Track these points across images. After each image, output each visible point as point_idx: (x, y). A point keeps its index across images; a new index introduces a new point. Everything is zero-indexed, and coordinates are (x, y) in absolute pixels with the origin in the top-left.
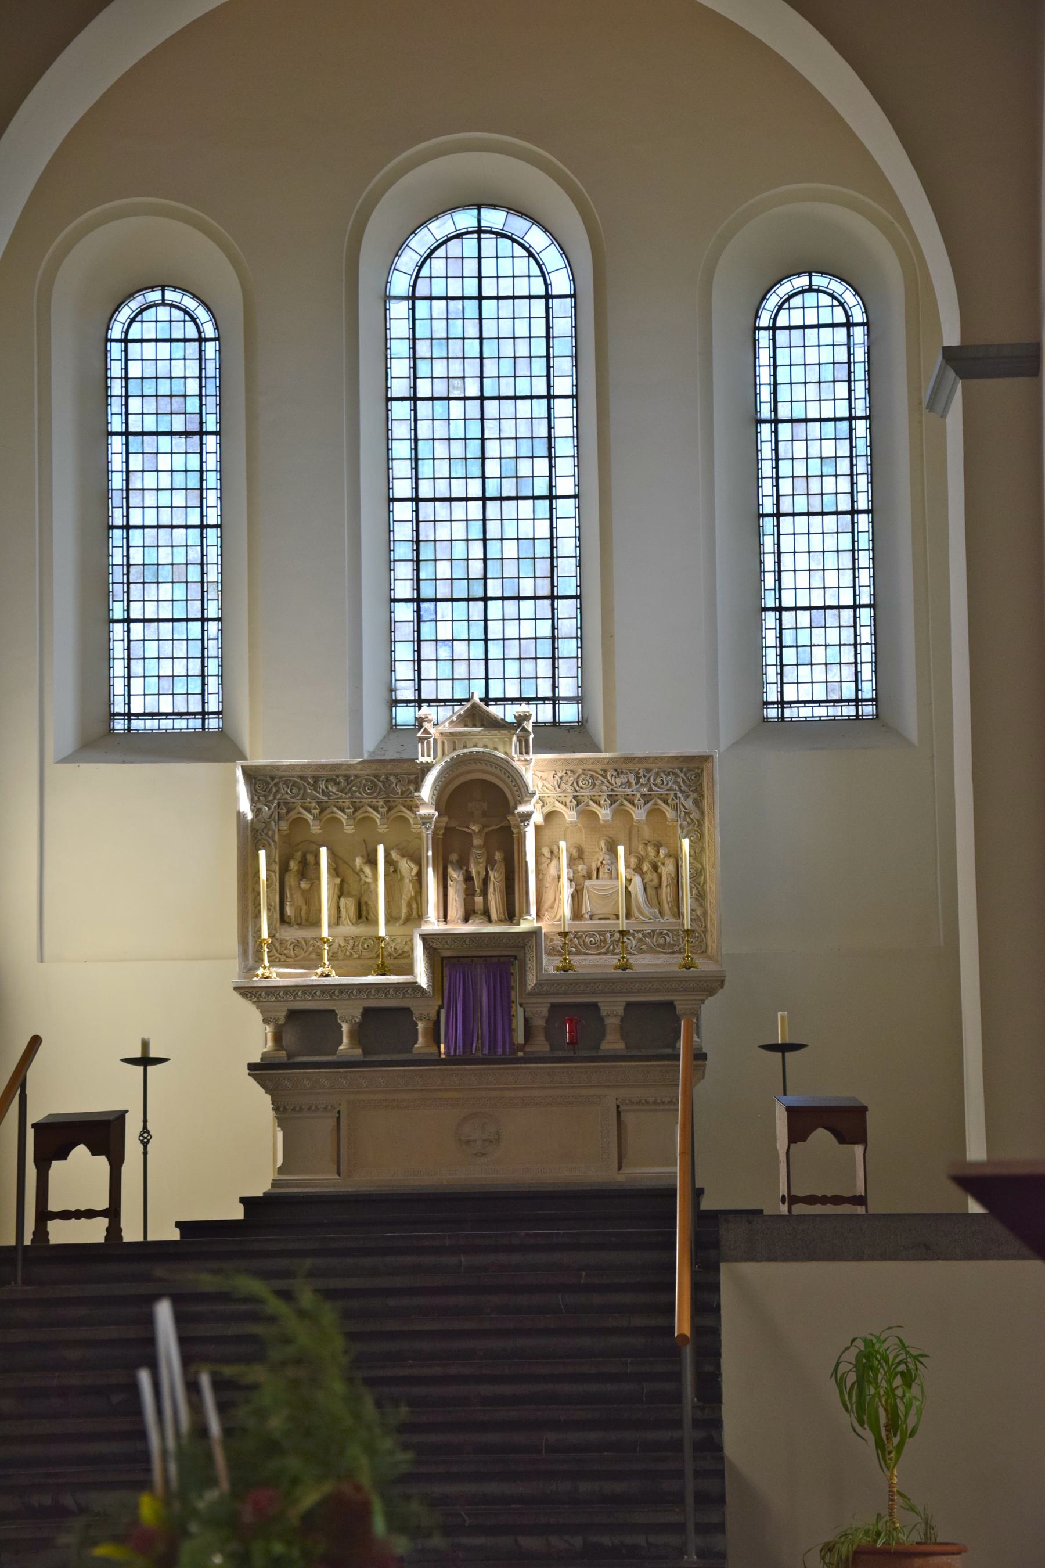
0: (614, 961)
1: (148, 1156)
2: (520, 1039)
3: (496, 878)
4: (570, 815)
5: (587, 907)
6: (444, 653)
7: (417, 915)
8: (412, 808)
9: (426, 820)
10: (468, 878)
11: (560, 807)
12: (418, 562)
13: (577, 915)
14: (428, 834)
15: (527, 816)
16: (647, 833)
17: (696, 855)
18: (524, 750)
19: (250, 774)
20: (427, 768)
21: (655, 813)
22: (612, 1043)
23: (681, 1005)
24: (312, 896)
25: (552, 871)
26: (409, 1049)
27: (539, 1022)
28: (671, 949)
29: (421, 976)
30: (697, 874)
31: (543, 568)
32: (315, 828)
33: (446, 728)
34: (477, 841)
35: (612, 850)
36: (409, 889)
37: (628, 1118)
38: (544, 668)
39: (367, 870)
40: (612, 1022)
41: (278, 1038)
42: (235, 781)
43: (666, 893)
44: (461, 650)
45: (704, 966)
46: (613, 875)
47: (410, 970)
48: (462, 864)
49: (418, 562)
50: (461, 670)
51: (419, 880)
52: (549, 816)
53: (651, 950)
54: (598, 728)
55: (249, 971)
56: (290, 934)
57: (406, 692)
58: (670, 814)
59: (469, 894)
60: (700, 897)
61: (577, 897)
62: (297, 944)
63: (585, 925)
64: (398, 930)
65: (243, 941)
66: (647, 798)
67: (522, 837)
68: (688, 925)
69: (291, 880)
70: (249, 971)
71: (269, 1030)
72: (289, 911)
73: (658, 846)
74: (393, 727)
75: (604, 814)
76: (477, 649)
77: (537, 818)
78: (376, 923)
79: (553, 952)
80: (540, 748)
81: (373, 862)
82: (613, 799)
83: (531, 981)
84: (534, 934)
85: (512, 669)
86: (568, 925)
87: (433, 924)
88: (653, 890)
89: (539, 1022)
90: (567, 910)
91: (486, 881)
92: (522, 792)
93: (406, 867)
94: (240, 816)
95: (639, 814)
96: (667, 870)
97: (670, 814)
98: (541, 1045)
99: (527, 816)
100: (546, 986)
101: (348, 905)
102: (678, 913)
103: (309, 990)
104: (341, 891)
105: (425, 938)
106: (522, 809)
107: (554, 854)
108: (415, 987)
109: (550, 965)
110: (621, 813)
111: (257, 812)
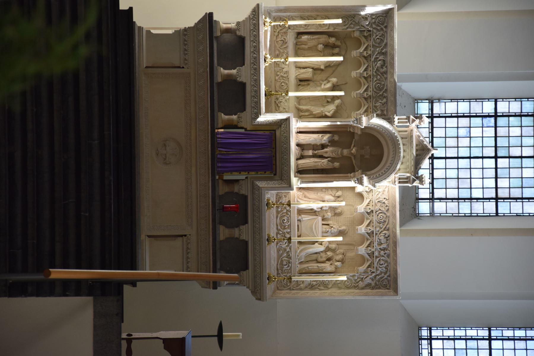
0: (273, 234)
1: (441, 137)
2: (227, 177)
3: (323, 163)
4: (361, 208)
5: (305, 218)
6: (463, 132)
7: (301, 115)
8: (366, 112)
9: (359, 121)
10: (323, 146)
11: (366, 202)
12: (520, 115)
13: (301, 212)
14: (350, 122)
15: (361, 182)
16: (350, 255)
17: (336, 284)
18: (401, 181)
19: (388, 14)
20: (391, 121)
21: (363, 260)
22: (223, 233)
23: (248, 274)
24: (313, 51)
25: (327, 197)
26: (220, 110)
27: (236, 189)
28: (280, 269)
29: (265, 118)
30: (325, 285)
31: (516, 193)
32: (355, 53)
33: (415, 133)
34: (346, 152)
35: (340, 233)
36: (317, 110)
37: (178, 242)
38: (453, 193)
39: (329, 85)
40: (236, 232)
41: (228, 31)
42: (385, 4)
43: (314, 266)
44: (465, 142)
45: (269, 288)
46: (325, 234)
47: (268, 110)
48: (332, 143)
49: (520, 115)
50: (451, 142)
51: (324, 117)
52: (361, 196)
53: (279, 256)
54: (415, 226)
55: (269, 14)
56: (291, 38)
57: (438, 108)
58: (362, 269)
59: (314, 147)
60: (311, 286)
61: (312, 212)
62: (284, 42)
63: (294, 216)
64: (292, 104)
65: (286, 9)
66: (371, 255)
67: (348, 179)
68: (294, 279)
69: (323, 39)
70: (269, 14)
71: (233, 25)
72: (305, 37)
73: (342, 261)
74: (417, 100)
75: (362, 229)
76: (464, 152)
77: (359, 188)
78: (297, 90)
79: (279, 197)
80: (404, 192)
81: (334, 88)
82: (371, 234)
83: (261, 184)
84: (290, 186)
85: (452, 173)
86: (295, 207)
87: (296, 125)
88: (315, 258)
89: (236, 189)
90: (304, 205)
91: (321, 157)
92: (375, 179)
93: (330, 109)
94: (363, 7)
95: (362, 250)
96: (327, 266)
97: (362, 269)
98: (222, 189)
99: (361, 182)
100: (257, 192)
101: (308, 74)
102: (301, 273)
103: (257, 50)
104: (316, 69)
105: (287, 120)
106: (365, 179)
107: (337, 198)
108: (258, 114)
109: (270, 195)
110: (362, 239)
111: (365, 18)
